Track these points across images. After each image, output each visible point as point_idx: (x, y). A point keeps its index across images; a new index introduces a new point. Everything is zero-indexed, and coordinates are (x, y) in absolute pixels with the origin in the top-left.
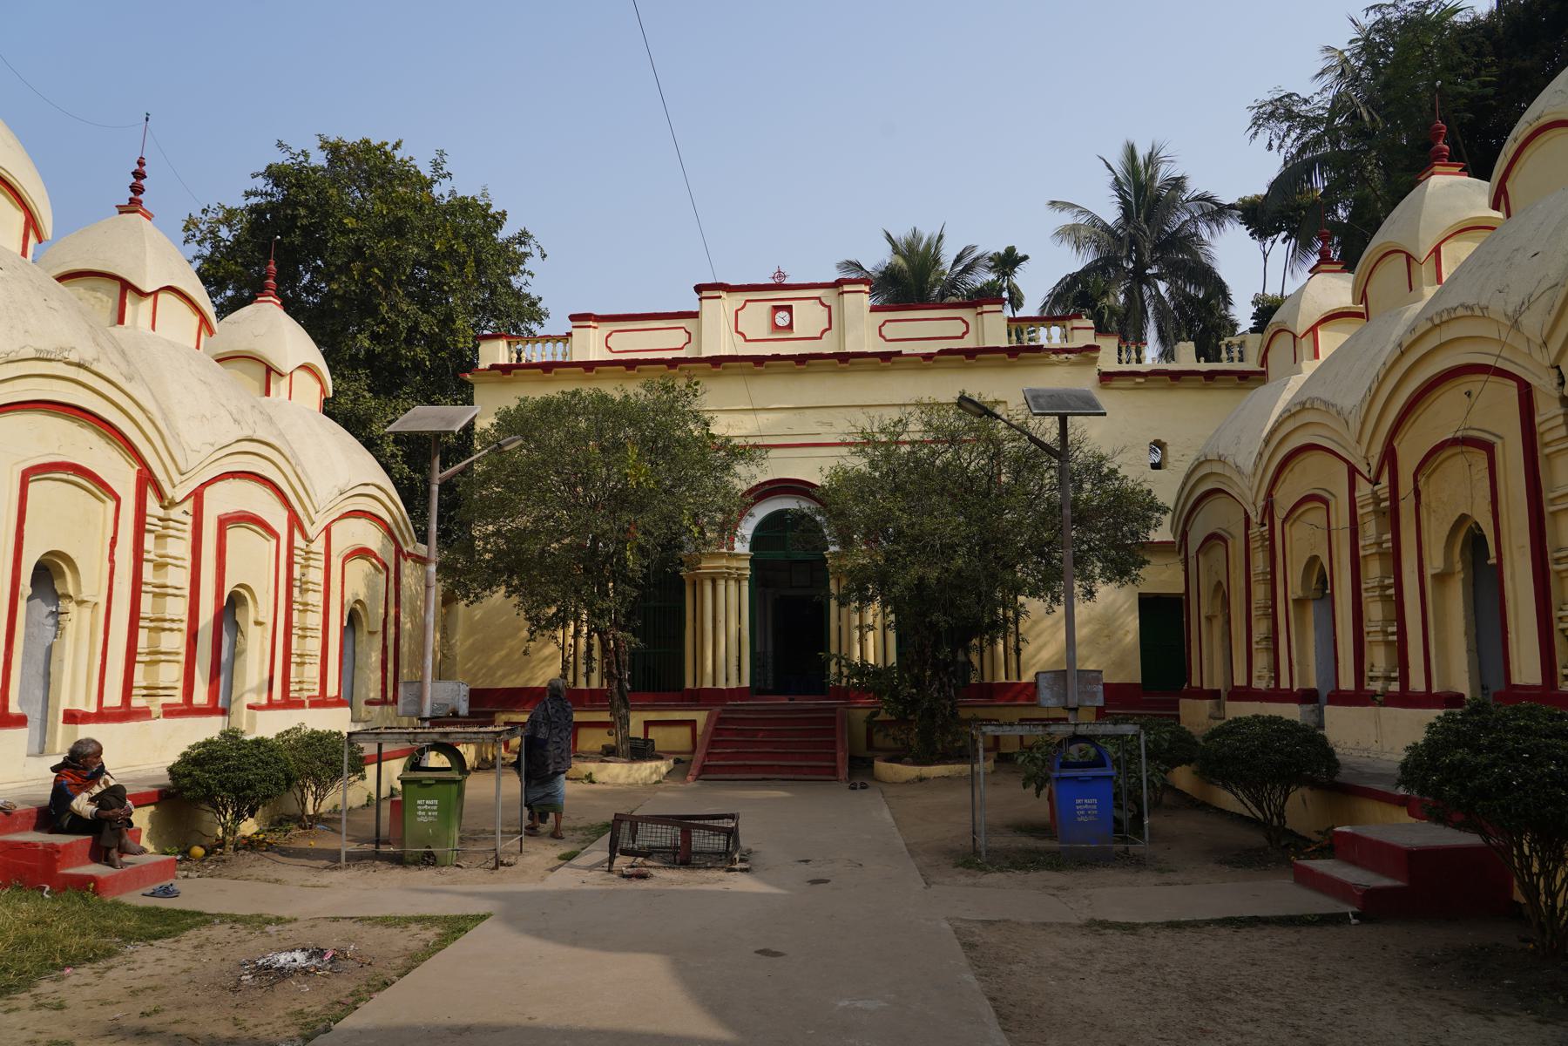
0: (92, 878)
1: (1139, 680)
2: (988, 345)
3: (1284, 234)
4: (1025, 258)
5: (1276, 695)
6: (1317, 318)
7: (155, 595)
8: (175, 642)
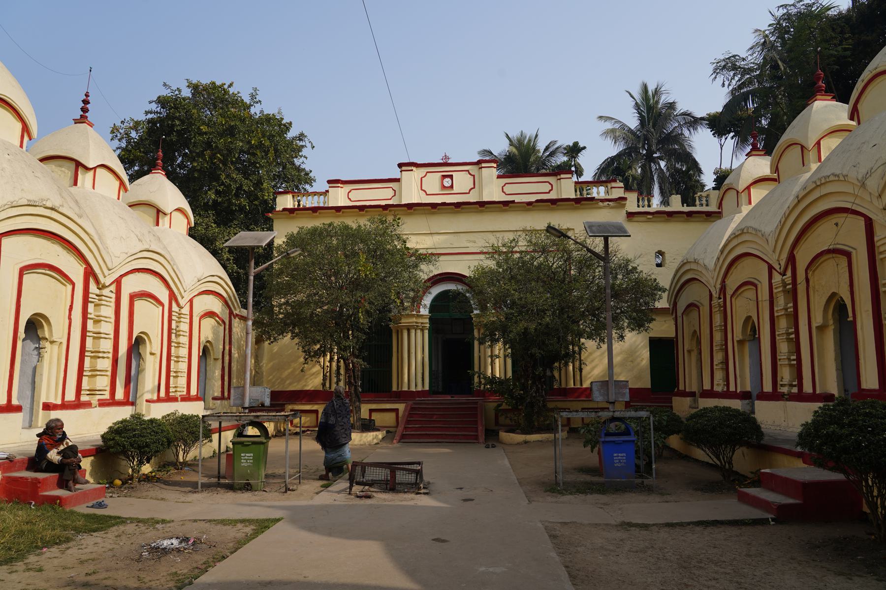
0: (58, 498)
2: (564, 197)
3: (732, 134)
4: (584, 148)
5: (727, 395)
6: (750, 181)
7: (94, 338)
8: (105, 364)
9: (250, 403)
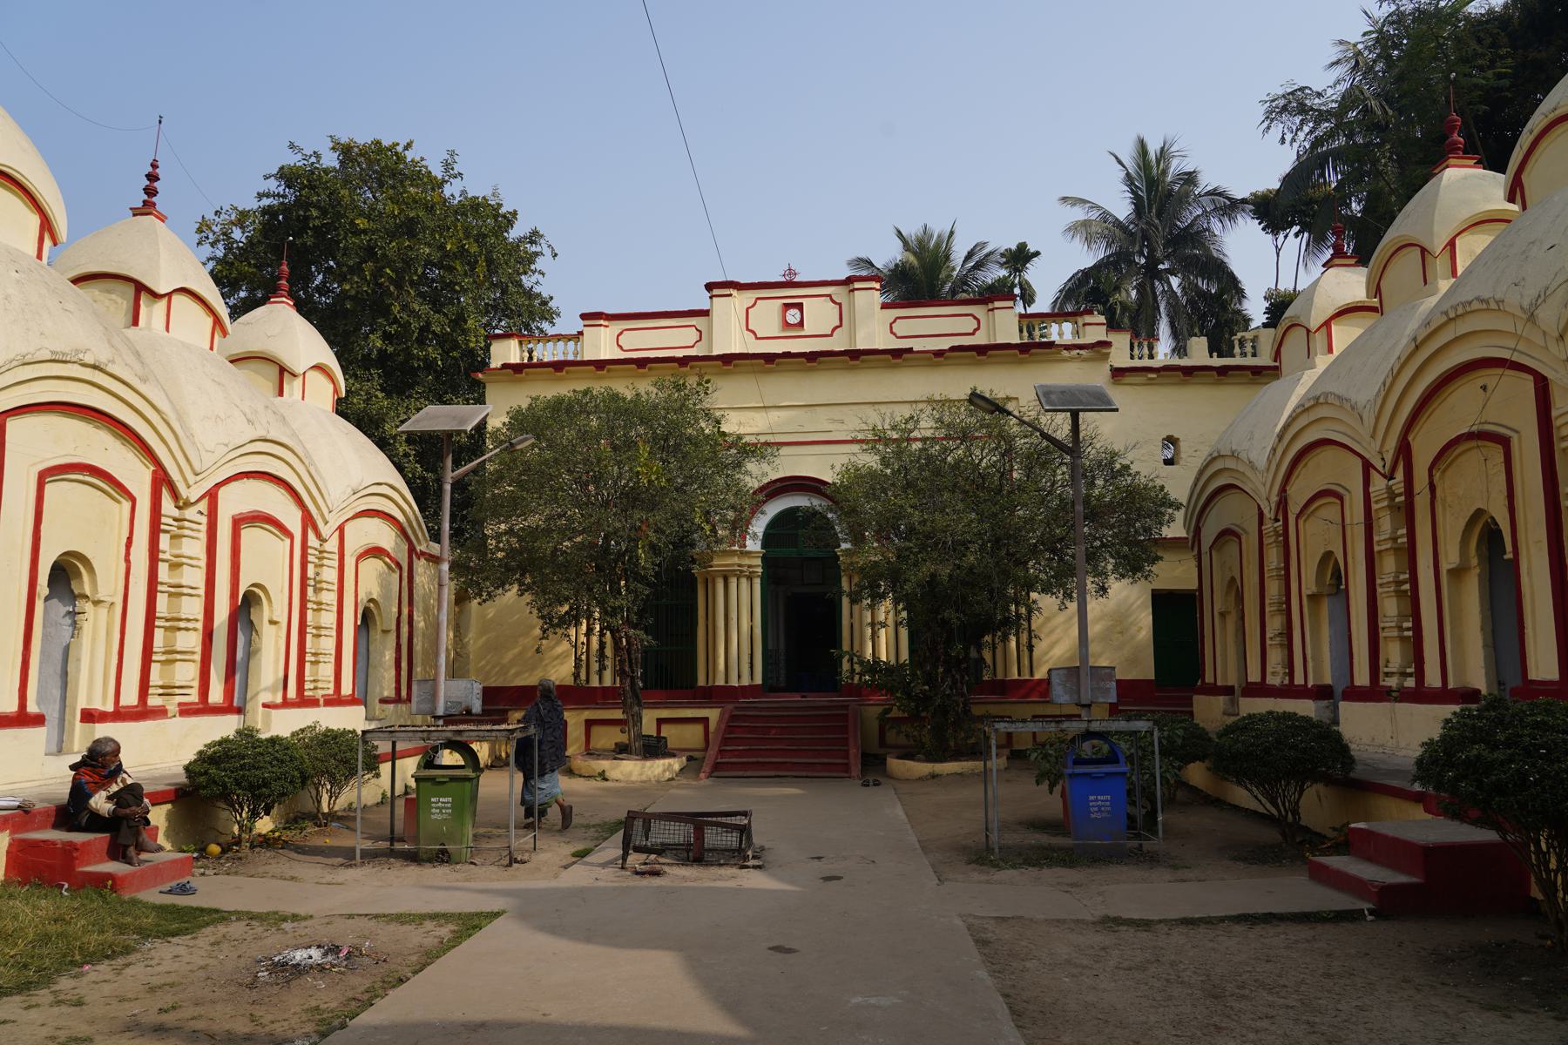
0: (109, 876)
1: (1150, 674)
3: (1296, 229)
4: (1037, 254)
5: (1290, 691)
6: (1331, 312)
7: (171, 595)
8: (191, 641)
9: (446, 709)
